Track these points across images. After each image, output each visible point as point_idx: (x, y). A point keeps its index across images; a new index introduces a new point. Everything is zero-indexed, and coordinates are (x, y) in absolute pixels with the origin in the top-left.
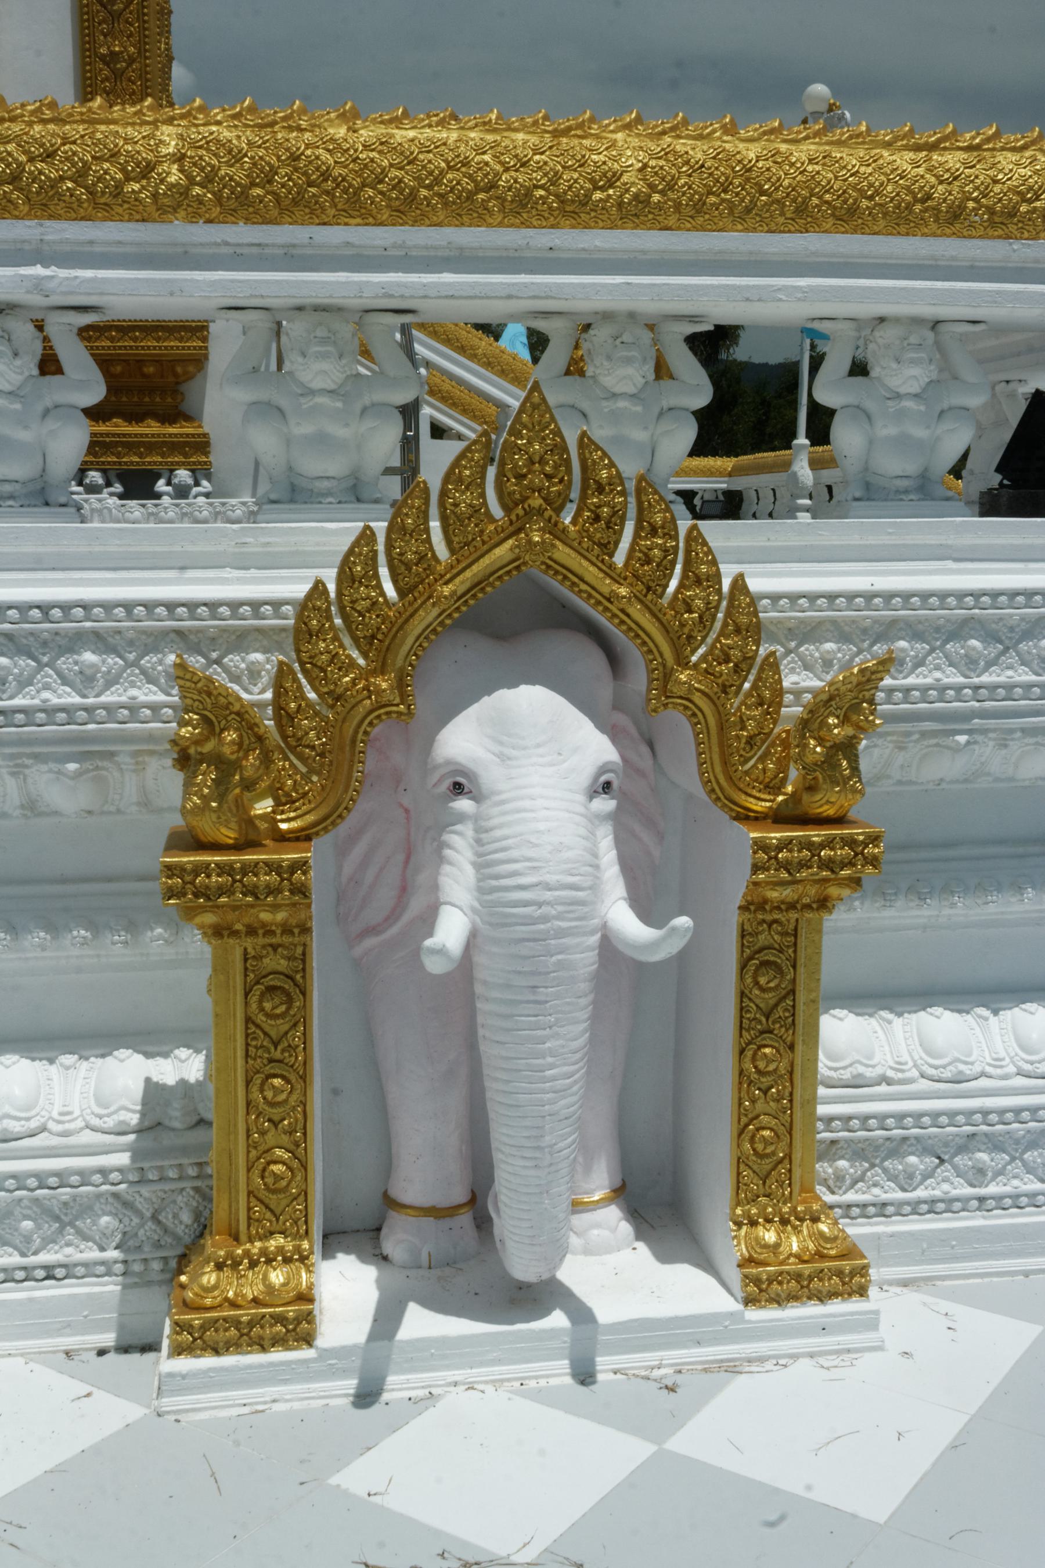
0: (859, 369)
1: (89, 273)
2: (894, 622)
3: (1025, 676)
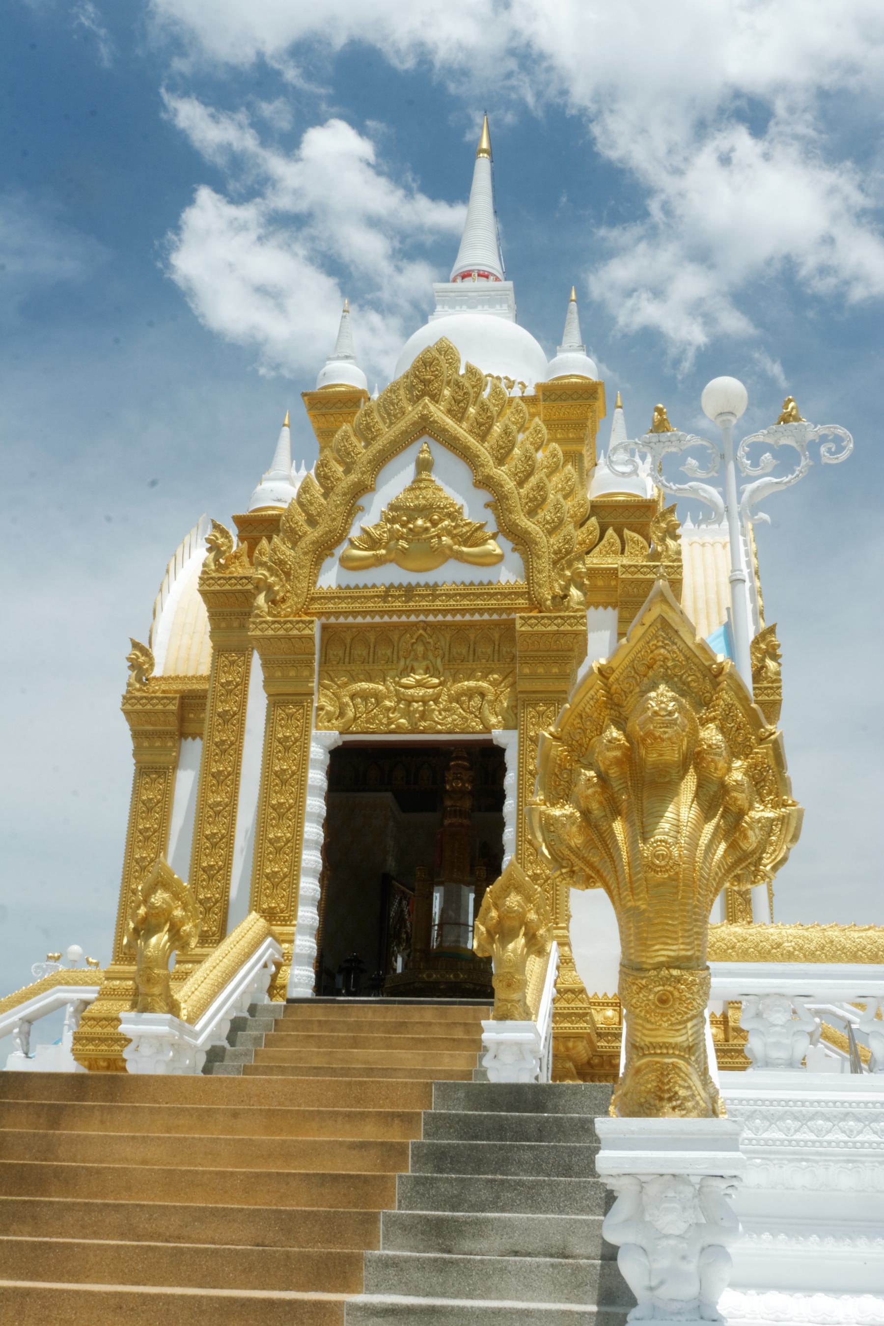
0: (758, 1015)
2: (817, 1113)
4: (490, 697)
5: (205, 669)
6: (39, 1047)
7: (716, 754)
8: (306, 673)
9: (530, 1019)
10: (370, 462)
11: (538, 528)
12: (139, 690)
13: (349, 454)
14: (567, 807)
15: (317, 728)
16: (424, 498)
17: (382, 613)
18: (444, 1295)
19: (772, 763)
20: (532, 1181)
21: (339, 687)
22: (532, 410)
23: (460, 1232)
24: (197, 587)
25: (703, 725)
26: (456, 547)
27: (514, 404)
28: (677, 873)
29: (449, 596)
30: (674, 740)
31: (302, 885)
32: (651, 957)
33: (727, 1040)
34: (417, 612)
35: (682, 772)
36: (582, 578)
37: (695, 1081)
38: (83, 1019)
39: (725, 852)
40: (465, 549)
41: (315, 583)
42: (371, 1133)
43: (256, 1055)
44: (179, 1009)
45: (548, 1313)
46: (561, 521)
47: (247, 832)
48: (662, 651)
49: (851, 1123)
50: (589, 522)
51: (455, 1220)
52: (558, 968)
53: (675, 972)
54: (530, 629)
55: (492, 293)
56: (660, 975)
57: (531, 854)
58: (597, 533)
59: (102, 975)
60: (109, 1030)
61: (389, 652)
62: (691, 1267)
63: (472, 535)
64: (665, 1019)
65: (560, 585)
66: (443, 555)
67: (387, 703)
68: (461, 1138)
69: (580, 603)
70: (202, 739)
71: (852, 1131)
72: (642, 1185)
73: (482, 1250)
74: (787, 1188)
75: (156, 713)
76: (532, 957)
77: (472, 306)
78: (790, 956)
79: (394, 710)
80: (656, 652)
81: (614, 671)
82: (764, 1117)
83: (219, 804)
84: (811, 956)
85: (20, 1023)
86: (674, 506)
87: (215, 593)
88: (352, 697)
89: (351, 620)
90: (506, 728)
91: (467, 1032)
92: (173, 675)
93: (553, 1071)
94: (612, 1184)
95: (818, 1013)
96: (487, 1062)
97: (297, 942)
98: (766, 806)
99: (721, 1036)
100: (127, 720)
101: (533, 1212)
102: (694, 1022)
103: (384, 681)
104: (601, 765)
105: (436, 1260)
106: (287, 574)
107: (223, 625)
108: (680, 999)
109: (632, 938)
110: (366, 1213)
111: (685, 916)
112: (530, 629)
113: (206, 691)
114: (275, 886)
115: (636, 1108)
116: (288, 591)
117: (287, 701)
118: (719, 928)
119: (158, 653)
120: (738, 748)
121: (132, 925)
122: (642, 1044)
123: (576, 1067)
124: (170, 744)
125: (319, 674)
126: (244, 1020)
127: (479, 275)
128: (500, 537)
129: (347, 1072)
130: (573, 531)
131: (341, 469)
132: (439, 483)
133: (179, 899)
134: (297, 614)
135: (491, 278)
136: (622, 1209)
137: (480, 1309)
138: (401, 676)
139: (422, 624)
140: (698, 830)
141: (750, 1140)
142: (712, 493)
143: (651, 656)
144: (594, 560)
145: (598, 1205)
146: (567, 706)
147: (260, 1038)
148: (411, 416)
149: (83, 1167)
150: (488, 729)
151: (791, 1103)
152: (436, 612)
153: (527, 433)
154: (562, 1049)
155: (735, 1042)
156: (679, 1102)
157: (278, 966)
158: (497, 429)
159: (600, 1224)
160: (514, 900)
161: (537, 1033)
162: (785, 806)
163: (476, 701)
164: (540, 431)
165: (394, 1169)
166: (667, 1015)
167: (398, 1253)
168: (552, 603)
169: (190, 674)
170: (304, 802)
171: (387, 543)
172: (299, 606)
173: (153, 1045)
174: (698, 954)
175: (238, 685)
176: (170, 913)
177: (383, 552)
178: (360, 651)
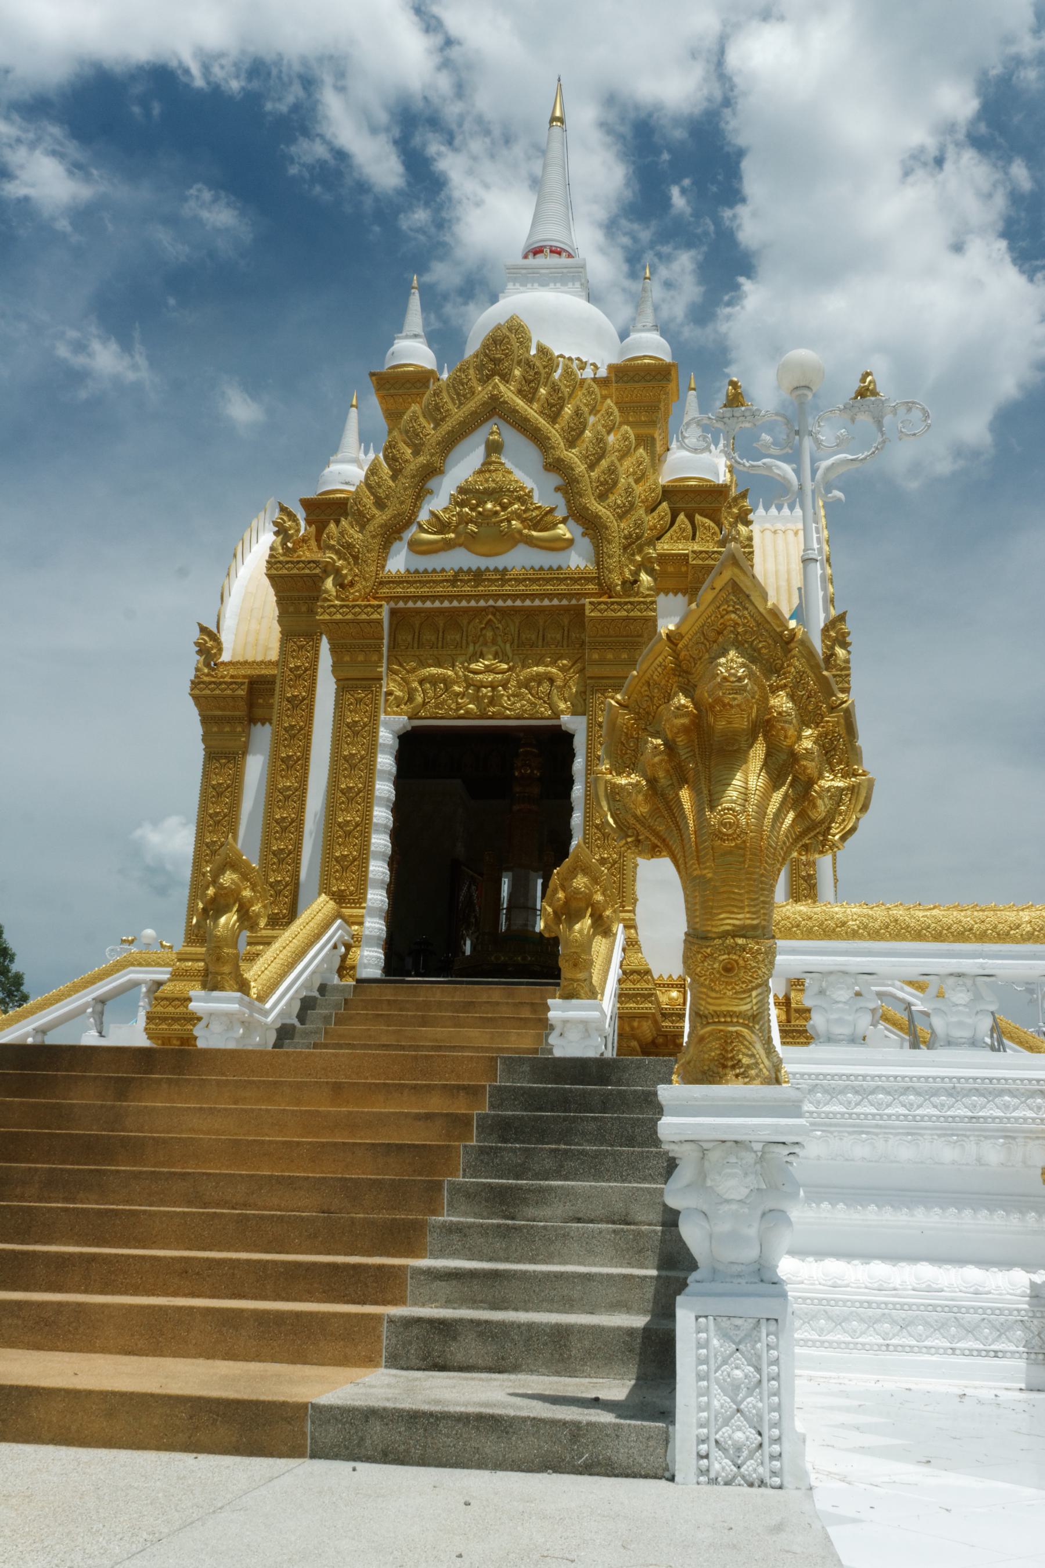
0: (822, 992)
1: (1000, 962)
2: (878, 1087)
3: (1030, 1114)
4: (559, 683)
5: (274, 655)
6: (112, 1026)
7: (785, 722)
8: (375, 658)
9: (596, 998)
10: (438, 444)
11: (608, 513)
12: (207, 675)
13: (418, 435)
14: (633, 776)
15: (386, 713)
16: (493, 481)
17: (451, 598)
18: (507, 1260)
19: (843, 732)
20: (596, 1151)
21: (408, 672)
22: (604, 392)
23: (525, 1201)
24: (265, 570)
25: (773, 692)
26: (526, 531)
27: (586, 386)
28: (744, 842)
29: (519, 581)
30: (744, 707)
31: (371, 868)
32: (716, 926)
33: (789, 1021)
34: (486, 597)
35: (751, 741)
36: (653, 563)
37: (759, 1049)
38: (156, 999)
39: (793, 821)
40: (534, 533)
41: (383, 567)
42: (436, 1104)
43: (326, 1033)
44: (249, 988)
45: (610, 1277)
46: (632, 505)
47: (316, 815)
48: (733, 616)
49: (912, 1097)
50: (660, 507)
51: (519, 1188)
52: (624, 950)
53: (740, 941)
54: (599, 614)
55: (565, 270)
56: (725, 947)
57: (599, 839)
58: (668, 518)
59: (174, 956)
60: (182, 1009)
61: (458, 637)
62: (752, 1232)
63: (541, 519)
64: (729, 988)
65: (630, 570)
66: (513, 540)
67: (456, 688)
68: (525, 1110)
69: (649, 589)
70: (271, 724)
71: (912, 1105)
72: (704, 1152)
73: (547, 1217)
74: (847, 1160)
75: (224, 698)
76: (598, 938)
77: (544, 284)
78: (854, 935)
79: (463, 695)
80: (726, 617)
81: (683, 637)
82: (825, 1091)
83: (288, 788)
84: (875, 935)
85: (93, 1003)
86: (747, 490)
87: (281, 576)
88: (421, 682)
89: (419, 604)
90: (574, 713)
91: (534, 1011)
92: (242, 660)
93: (618, 1049)
94: (674, 1150)
95: (880, 995)
96: (553, 1040)
97: (367, 924)
98: (835, 776)
99: (784, 1017)
100: (196, 705)
101: (595, 1180)
102: (759, 990)
103: (453, 666)
104: (668, 732)
105: (499, 1226)
106: (356, 558)
107: (291, 609)
108: (745, 967)
109: (697, 907)
110: (429, 1181)
111: (751, 885)
112: (599, 614)
113: (274, 676)
114: (344, 869)
115: (700, 1076)
116: (356, 575)
117: (355, 685)
118: (786, 908)
119: (226, 638)
120: (808, 717)
121: (201, 905)
122: (706, 1012)
123: (641, 1046)
124: (239, 729)
125: (388, 659)
126: (314, 999)
127: (551, 251)
128: (571, 521)
129: (417, 1048)
130: (644, 516)
131: (409, 451)
132: (509, 465)
133: (248, 880)
134: (366, 598)
135: (564, 254)
136: (684, 1175)
137: (542, 1273)
138: (470, 662)
139: (491, 609)
140: (766, 797)
141: (811, 1113)
142: (787, 470)
143: (722, 621)
144: (665, 546)
145: (660, 1174)
146: (635, 673)
147: (331, 1016)
148: (480, 396)
149: (150, 1138)
150: (556, 715)
151: (852, 1078)
152: (505, 597)
153: (599, 415)
154: (627, 1029)
155: (797, 1022)
156: (742, 1070)
157: (348, 947)
158: (568, 410)
159: (661, 1192)
160: (580, 882)
161: (602, 1012)
162: (855, 775)
163: (545, 687)
164: (612, 413)
165: (459, 1138)
166: (731, 983)
167: (462, 1219)
168: (622, 588)
169: (259, 659)
170: (373, 786)
171: (457, 527)
172: (367, 590)
173: (221, 1019)
174: (763, 923)
175: (306, 670)
176: (239, 893)
177: (452, 535)
178: (428, 636)
